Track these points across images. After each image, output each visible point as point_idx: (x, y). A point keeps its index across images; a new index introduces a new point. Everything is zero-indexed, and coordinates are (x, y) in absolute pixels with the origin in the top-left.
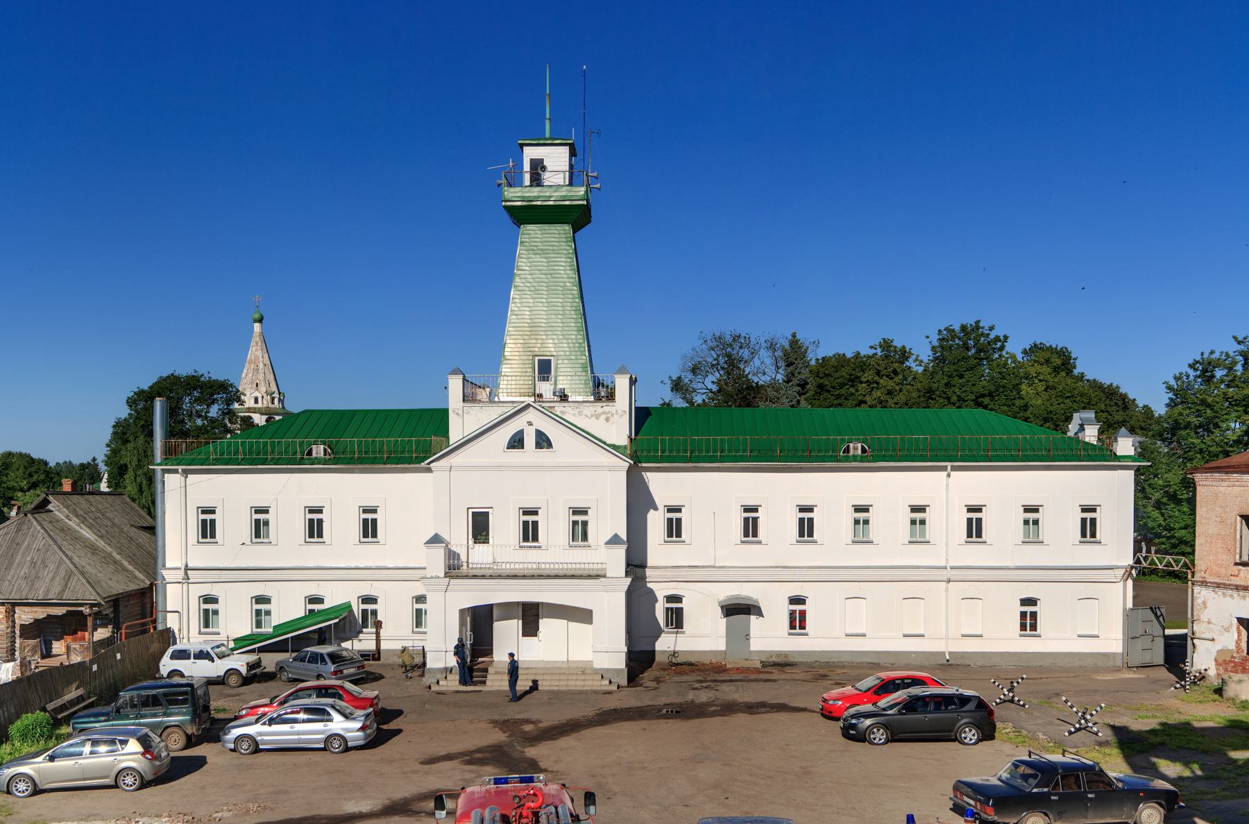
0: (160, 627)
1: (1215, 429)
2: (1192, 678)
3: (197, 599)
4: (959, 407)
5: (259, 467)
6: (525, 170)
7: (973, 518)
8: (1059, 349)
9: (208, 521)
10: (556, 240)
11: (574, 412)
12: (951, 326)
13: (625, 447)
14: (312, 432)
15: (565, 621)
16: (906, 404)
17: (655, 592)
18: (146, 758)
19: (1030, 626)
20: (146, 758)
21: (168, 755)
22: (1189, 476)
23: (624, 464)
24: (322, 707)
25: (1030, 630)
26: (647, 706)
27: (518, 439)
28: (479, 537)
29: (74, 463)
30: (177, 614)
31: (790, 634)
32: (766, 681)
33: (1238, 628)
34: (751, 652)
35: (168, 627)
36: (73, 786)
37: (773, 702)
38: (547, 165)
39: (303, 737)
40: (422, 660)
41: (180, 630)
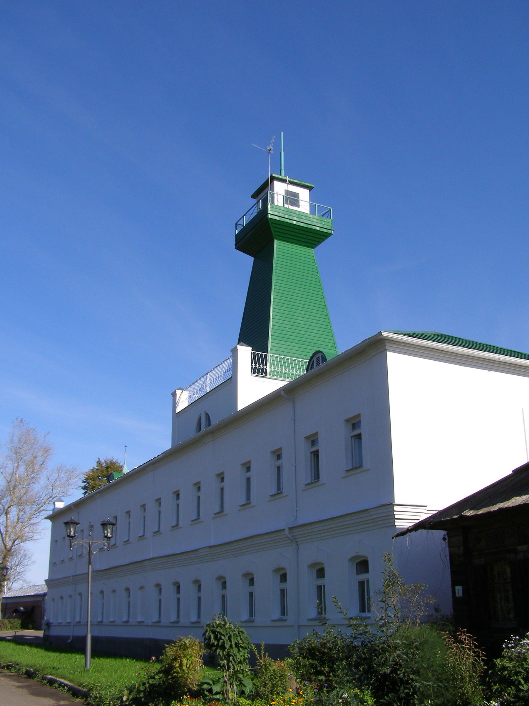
0: (45, 590)
3: (350, 438)
5: (283, 153)
6: (289, 206)
7: (364, 581)
8: (283, 661)
10: (301, 305)
13: (163, 676)
17: (238, 350)
18: (454, 591)
20: (454, 591)
22: (45, 676)
23: (317, 609)
24: (323, 603)
25: (263, 354)
27: (394, 539)
28: (108, 705)
29: (47, 578)
31: (369, 578)
32: (388, 526)
33: (419, 520)
34: (43, 637)
35: (44, 583)
40: (88, 571)
41: (179, 399)
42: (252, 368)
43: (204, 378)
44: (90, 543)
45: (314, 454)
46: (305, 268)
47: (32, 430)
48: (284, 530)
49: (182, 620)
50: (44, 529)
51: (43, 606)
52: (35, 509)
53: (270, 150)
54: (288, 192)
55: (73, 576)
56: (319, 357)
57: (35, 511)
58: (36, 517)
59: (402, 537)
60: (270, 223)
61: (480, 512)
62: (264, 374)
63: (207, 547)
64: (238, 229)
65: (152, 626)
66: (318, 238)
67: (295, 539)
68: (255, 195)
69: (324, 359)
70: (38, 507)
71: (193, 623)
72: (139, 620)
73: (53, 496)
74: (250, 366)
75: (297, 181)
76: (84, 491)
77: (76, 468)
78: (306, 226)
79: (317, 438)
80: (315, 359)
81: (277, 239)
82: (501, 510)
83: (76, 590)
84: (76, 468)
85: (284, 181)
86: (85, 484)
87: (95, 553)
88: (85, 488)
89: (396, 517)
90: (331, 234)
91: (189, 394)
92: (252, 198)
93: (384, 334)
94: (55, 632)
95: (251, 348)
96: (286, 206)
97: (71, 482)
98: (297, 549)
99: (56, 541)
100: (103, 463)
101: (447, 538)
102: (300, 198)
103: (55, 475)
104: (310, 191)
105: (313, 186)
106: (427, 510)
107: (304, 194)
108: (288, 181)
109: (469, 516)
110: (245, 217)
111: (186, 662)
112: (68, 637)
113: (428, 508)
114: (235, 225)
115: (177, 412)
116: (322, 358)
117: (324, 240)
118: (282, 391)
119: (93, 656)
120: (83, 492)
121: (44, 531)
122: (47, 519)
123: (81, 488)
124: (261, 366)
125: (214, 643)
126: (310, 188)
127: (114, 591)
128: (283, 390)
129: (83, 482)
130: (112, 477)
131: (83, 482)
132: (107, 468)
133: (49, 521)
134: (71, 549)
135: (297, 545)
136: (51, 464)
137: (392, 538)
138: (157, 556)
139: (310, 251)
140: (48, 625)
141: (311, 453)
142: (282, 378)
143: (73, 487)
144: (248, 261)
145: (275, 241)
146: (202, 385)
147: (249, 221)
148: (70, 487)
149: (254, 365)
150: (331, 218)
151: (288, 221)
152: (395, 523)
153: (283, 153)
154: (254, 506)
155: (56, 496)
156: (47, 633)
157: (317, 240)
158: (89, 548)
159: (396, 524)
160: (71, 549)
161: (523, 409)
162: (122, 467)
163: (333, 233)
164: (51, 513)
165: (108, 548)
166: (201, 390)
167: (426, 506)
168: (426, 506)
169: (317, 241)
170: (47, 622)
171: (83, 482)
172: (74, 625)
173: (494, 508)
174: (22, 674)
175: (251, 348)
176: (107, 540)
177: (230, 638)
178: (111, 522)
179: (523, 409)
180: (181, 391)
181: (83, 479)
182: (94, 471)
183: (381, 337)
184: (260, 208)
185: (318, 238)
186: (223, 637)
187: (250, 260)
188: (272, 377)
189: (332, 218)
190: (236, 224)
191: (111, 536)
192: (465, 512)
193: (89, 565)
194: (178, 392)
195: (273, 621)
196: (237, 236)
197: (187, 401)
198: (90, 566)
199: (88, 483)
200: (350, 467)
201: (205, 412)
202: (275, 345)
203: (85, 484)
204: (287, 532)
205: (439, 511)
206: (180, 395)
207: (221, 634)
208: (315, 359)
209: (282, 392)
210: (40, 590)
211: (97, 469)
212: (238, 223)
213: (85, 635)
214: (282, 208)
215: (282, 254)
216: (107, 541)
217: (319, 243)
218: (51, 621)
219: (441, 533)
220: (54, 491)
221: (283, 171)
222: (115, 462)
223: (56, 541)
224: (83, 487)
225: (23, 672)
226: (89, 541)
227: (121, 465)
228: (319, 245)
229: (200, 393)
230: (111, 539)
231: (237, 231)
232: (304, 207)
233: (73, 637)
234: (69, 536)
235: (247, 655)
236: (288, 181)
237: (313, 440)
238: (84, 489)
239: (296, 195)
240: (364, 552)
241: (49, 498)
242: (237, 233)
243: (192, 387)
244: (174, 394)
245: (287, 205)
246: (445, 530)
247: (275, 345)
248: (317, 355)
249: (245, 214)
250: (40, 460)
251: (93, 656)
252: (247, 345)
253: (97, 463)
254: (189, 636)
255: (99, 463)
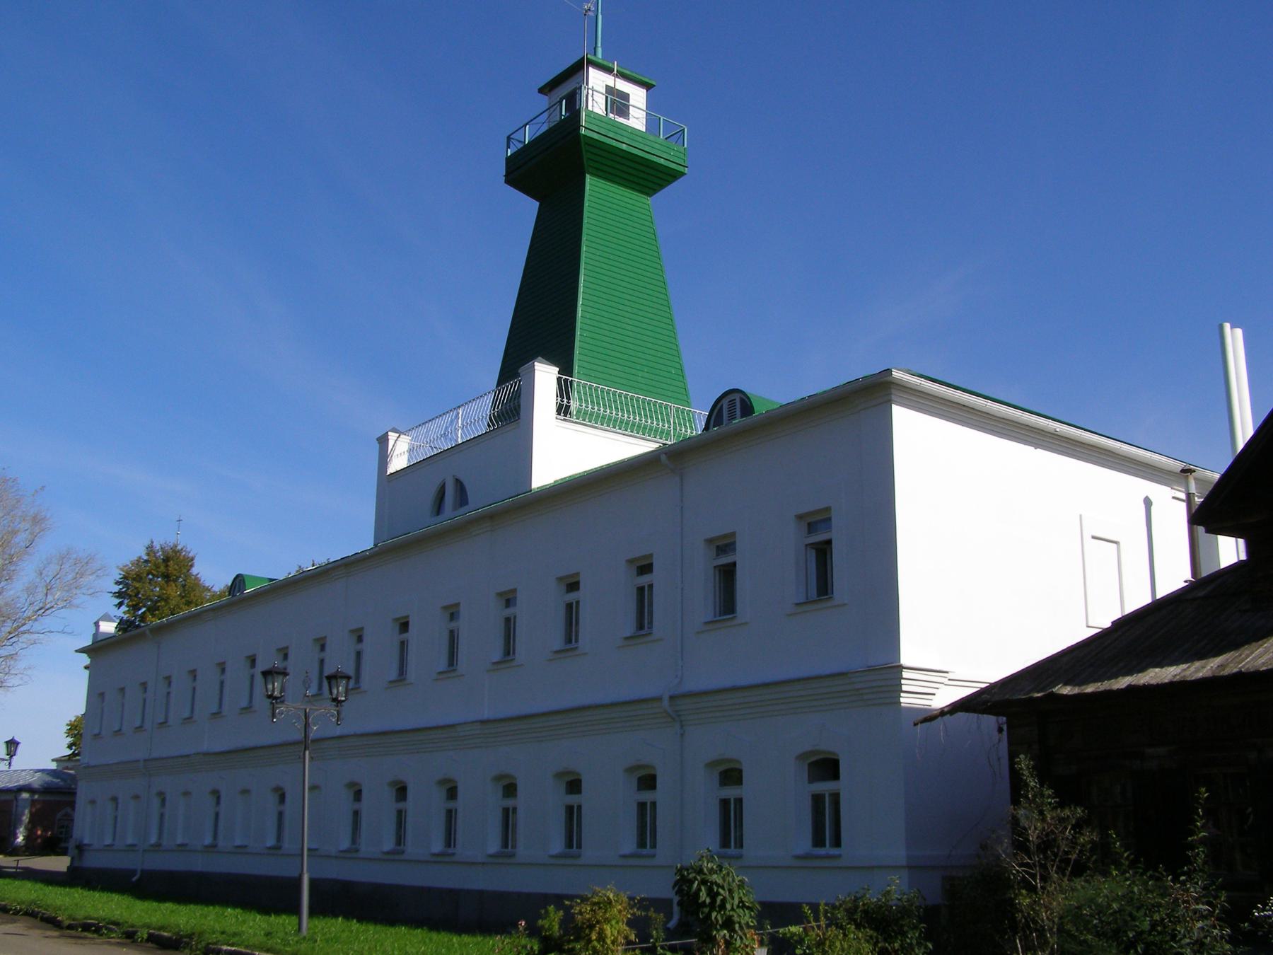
1: (1057, 873)
2: (90, 906)
4: (36, 620)
6: (616, 116)
9: (732, 802)
11: (731, 913)
12: (290, 574)
14: (809, 573)
15: (1222, 473)
16: (12, 756)
17: (536, 371)
19: (825, 840)
21: (840, 940)
26: (118, 763)
30: (1115, 545)
36: (564, 85)
37: (1224, 655)
38: (171, 540)
39: (1132, 466)
42: (557, 403)
43: (454, 413)
44: (308, 710)
45: (720, 571)
46: (616, 230)
47: (11, 480)
48: (659, 699)
49: (221, 843)
50: (30, 668)
51: (14, 810)
52: (8, 629)
53: (589, 10)
54: (610, 90)
55: (145, 760)
56: (735, 400)
57: (10, 633)
58: (12, 645)
59: (928, 724)
60: (583, 144)
61: (1090, 689)
62: (581, 419)
63: (476, 722)
64: (511, 147)
65: (483, 863)
66: (661, 179)
67: (679, 716)
68: (548, 88)
69: (747, 408)
70: (14, 626)
71: (434, 855)
72: (238, 842)
73: (48, 606)
74: (555, 402)
75: (628, 72)
76: (117, 601)
77: (94, 556)
78: (642, 156)
79: (732, 540)
80: (725, 403)
81: (591, 174)
82: (1131, 689)
83: (149, 787)
84: (94, 556)
85: (609, 70)
86: (121, 587)
87: (315, 728)
88: (119, 595)
89: (904, 688)
90: (683, 174)
91: (411, 440)
92: (539, 92)
93: (896, 374)
94: (93, 861)
95: (558, 369)
96: (611, 116)
97: (84, 581)
98: (682, 735)
99: (102, 694)
100: (158, 552)
101: (1005, 727)
102: (631, 102)
103: (54, 568)
104: (647, 91)
105: (654, 83)
106: (949, 680)
107: (638, 96)
108: (615, 72)
109: (1066, 695)
110: (528, 126)
111: (609, 930)
112: (134, 872)
113: (951, 676)
114: (506, 140)
115: (388, 473)
116: (741, 405)
117: (669, 183)
118: (664, 455)
119: (313, 912)
120: (117, 603)
121: (29, 672)
122: (80, 652)
123: (111, 595)
124: (565, 400)
125: (705, 901)
126: (648, 86)
127: (245, 792)
128: (666, 454)
129: (118, 583)
130: (240, 583)
131: (116, 583)
132: (166, 560)
133: (84, 655)
134: (275, 720)
135: (682, 726)
136: (47, 547)
137: (913, 724)
138: (352, 733)
139: (644, 201)
140: (81, 848)
141: (715, 567)
142: (599, 425)
143: (84, 591)
144: (528, 208)
145: (588, 176)
146: (447, 428)
147: (538, 134)
148: (78, 591)
149: (559, 399)
150: (684, 145)
151: (614, 143)
152: (901, 699)
153: (600, 17)
154: (585, 654)
155: (53, 607)
156: (77, 864)
157: (656, 180)
158: (306, 719)
159: (902, 700)
160: (275, 720)
161: (1081, 516)
162: (192, 559)
163: (686, 172)
164: (89, 643)
165: (338, 721)
166: (445, 435)
167: (947, 672)
168: (947, 672)
169: (659, 185)
170: (78, 843)
171: (118, 583)
172: (144, 851)
173: (1123, 682)
174: (141, 941)
175: (558, 369)
176: (337, 706)
177: (730, 891)
178: (344, 673)
179: (1081, 516)
180: (397, 435)
181: (118, 577)
182: (140, 564)
183: (889, 379)
184: (564, 113)
185: (661, 179)
186: (720, 890)
187: (538, 203)
188: (580, 420)
189: (686, 146)
190: (509, 138)
191: (343, 699)
192: (1057, 688)
193: (305, 750)
194: (392, 436)
195: (624, 856)
196: (508, 160)
197: (406, 456)
198: (307, 752)
199: (127, 585)
200: (802, 599)
201: (454, 476)
202: (586, 365)
203: (121, 587)
204: (666, 703)
205: (991, 684)
206: (395, 442)
207: (718, 886)
208: (725, 403)
209: (663, 457)
210: (6, 780)
211: (146, 561)
212: (512, 137)
213: (296, 875)
214: (604, 119)
215: (597, 200)
216: (337, 709)
217: (662, 187)
218: (86, 841)
219: (990, 721)
220: (50, 598)
221: (599, 50)
222: (182, 549)
223: (102, 694)
224: (115, 593)
225: (143, 938)
226: (305, 707)
227: (191, 555)
228: (660, 190)
229: (442, 442)
230: (343, 704)
231: (509, 150)
232: (637, 120)
233: (142, 871)
234: (270, 697)
235: (753, 922)
236: (615, 72)
237: (724, 545)
238: (117, 597)
239: (625, 97)
240: (828, 745)
241: (38, 610)
242: (509, 155)
243: (423, 430)
244: (383, 440)
245: (613, 115)
246: (997, 714)
247: (586, 365)
248: (733, 395)
249: (530, 122)
250: (21, 539)
251: (313, 912)
252: (547, 362)
253: (147, 548)
254: (608, 887)
255: (150, 549)
